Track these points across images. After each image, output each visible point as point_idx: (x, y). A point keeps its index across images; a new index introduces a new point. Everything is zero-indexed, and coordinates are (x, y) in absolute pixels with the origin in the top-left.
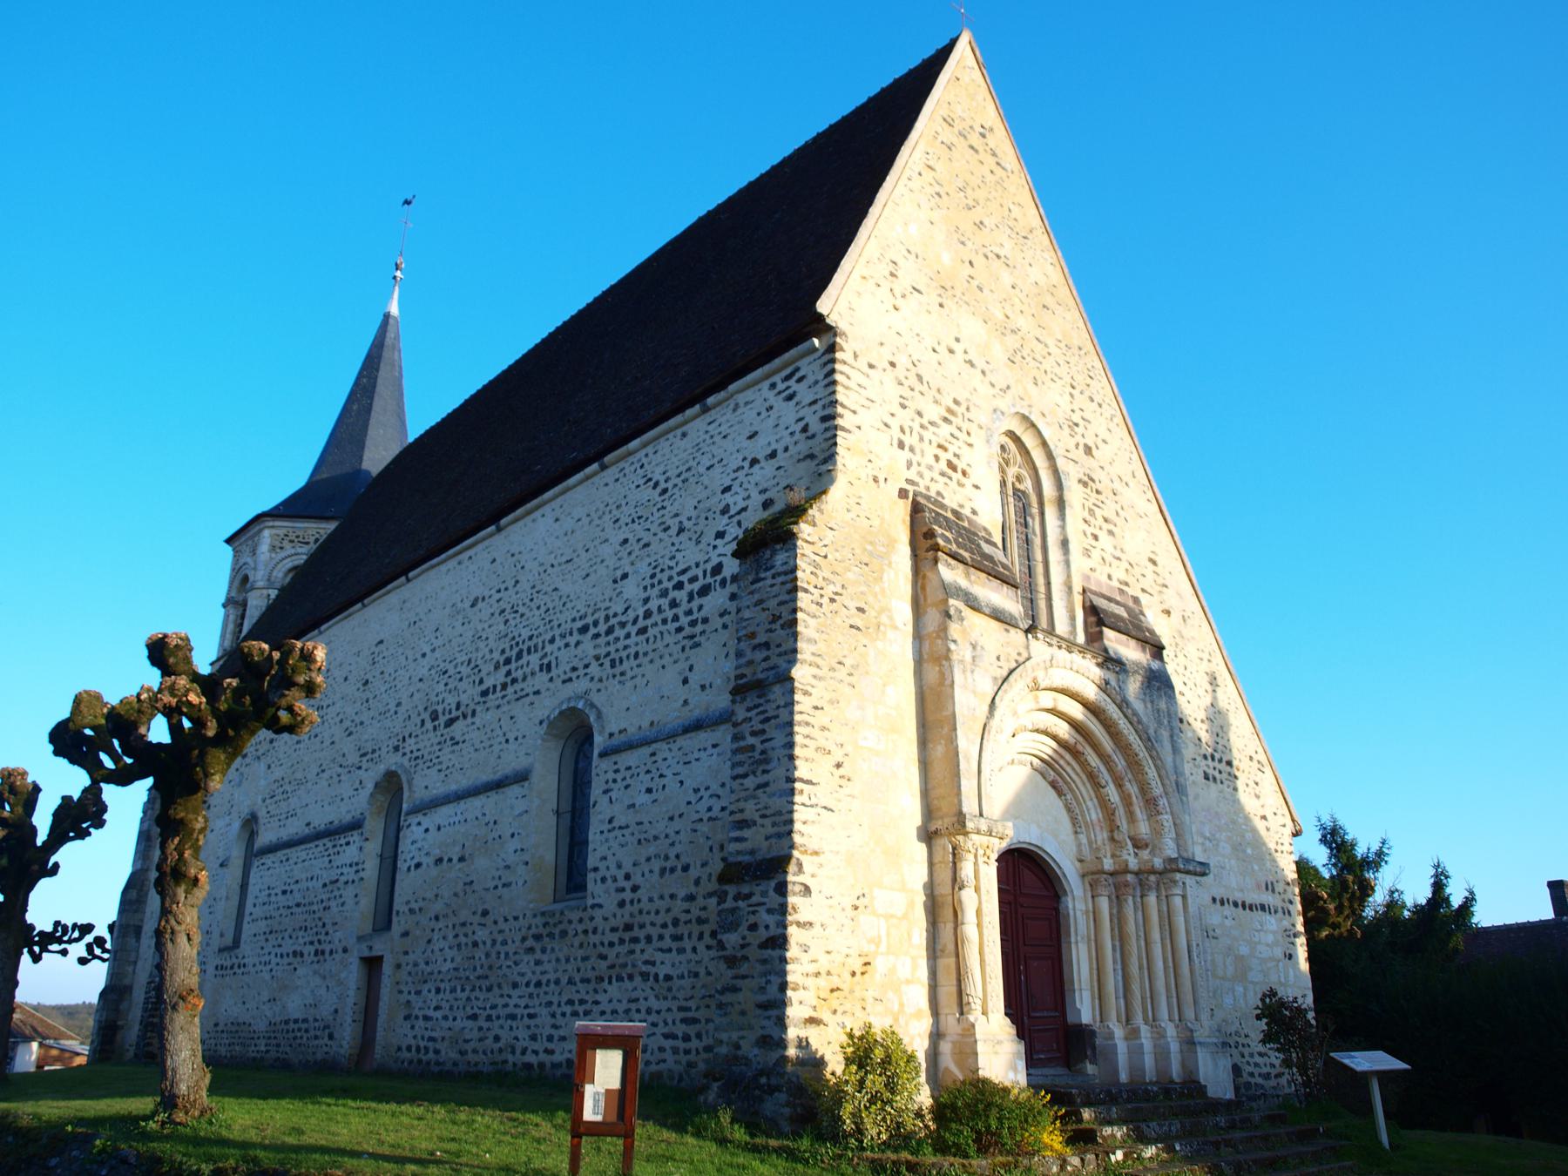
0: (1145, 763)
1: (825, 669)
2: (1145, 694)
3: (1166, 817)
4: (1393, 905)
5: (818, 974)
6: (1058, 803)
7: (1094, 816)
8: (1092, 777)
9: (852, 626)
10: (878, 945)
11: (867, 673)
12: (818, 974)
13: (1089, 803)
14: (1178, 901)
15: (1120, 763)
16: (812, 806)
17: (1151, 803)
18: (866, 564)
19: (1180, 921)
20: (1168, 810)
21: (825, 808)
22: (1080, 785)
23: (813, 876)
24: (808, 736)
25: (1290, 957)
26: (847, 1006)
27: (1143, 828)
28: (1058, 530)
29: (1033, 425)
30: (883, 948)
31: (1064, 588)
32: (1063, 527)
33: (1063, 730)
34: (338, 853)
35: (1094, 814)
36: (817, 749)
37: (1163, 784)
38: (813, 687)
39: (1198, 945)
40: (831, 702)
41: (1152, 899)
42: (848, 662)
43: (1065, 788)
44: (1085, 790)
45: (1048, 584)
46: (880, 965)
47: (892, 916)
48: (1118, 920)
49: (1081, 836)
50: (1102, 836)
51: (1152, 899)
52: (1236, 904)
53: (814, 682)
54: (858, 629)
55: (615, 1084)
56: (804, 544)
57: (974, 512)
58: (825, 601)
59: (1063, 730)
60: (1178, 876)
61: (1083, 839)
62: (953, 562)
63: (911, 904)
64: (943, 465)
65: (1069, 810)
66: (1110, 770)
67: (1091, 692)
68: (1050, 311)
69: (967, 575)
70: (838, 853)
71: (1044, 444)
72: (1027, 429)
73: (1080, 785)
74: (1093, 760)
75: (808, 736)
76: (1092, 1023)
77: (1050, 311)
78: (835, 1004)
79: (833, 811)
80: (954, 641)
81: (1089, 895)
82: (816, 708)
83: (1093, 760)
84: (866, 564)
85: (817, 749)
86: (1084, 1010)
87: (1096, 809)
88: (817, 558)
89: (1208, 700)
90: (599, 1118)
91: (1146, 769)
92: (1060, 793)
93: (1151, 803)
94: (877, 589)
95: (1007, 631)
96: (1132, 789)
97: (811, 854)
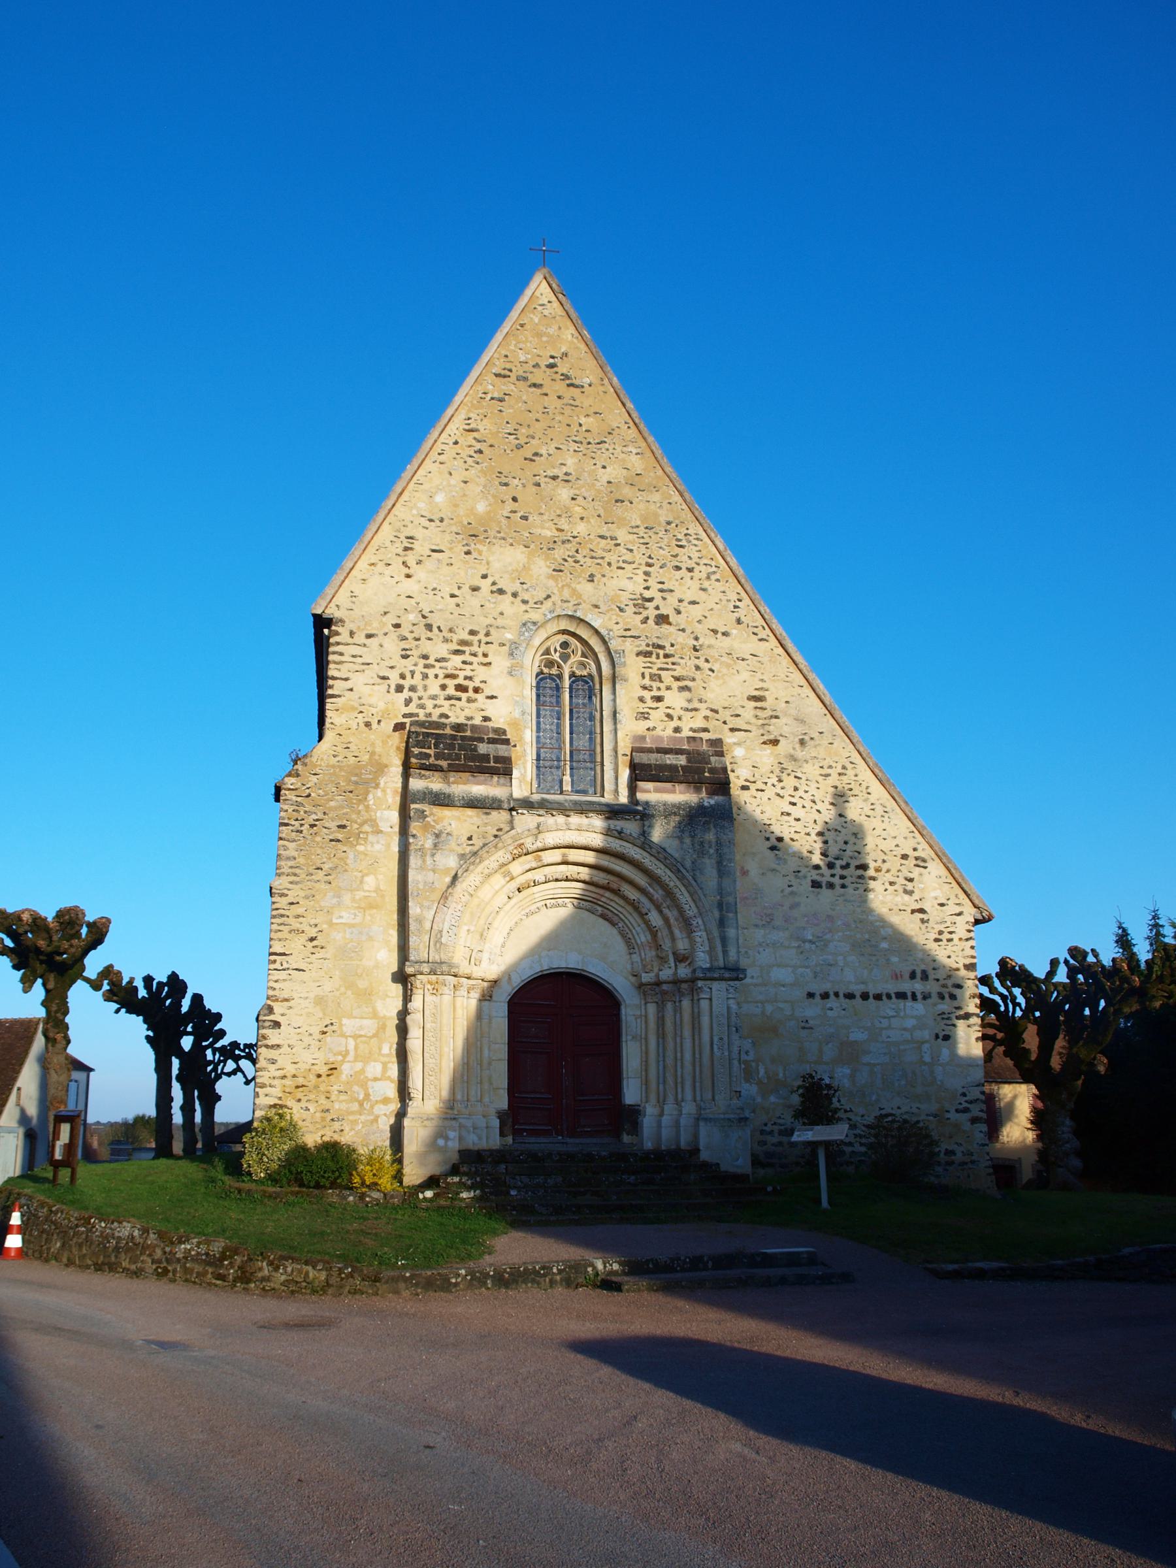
0: (676, 890)
1: (303, 876)
2: (682, 831)
3: (699, 934)
4: (148, 1029)
5: (284, 1077)
6: (615, 931)
7: (643, 939)
8: (635, 905)
9: (331, 840)
10: (345, 1056)
11: (346, 871)
12: (284, 1077)
13: (638, 929)
14: (704, 1004)
15: (658, 894)
16: (284, 970)
17: (687, 924)
18: (351, 792)
19: (705, 1020)
20: (702, 927)
21: (296, 969)
22: (627, 915)
23: (282, 1015)
24: (281, 924)
25: (947, 1038)
26: (312, 1097)
27: (682, 945)
28: (611, 703)
29: (582, 620)
30: (351, 1057)
31: (613, 753)
32: (614, 700)
33: (584, 873)
34: (913, 976)
35: (643, 937)
36: (290, 932)
37: (697, 907)
38: (289, 890)
39: (721, 1039)
40: (306, 897)
41: (686, 1003)
42: (326, 867)
43: (615, 919)
44: (633, 919)
45: (602, 751)
46: (346, 1069)
47: (361, 1036)
48: (661, 1020)
49: (634, 956)
50: (651, 954)
51: (686, 1003)
52: (850, 996)
53: (290, 886)
54: (338, 841)
55: (67, 1141)
56: (287, 792)
57: (486, 719)
58: (306, 827)
59: (584, 873)
60: (700, 984)
61: (636, 958)
62: (427, 773)
63: (383, 1027)
64: (451, 691)
65: (623, 935)
66: (651, 899)
67: (597, 840)
68: (627, 503)
69: (446, 780)
70: (307, 998)
71: (597, 632)
72: (578, 626)
73: (627, 915)
74: (632, 894)
75: (281, 924)
76: (639, 1103)
77: (627, 503)
78: (299, 1095)
79: (304, 971)
80: (414, 836)
81: (643, 1002)
82: (292, 903)
83: (632, 894)
84: (351, 792)
85: (290, 932)
86: (631, 1094)
87: (644, 932)
88: (299, 799)
89: (828, 814)
90: (60, 1158)
91: (678, 895)
92: (613, 924)
93: (687, 924)
94: (361, 807)
95: (487, 814)
96: (672, 915)
97: (282, 1001)
